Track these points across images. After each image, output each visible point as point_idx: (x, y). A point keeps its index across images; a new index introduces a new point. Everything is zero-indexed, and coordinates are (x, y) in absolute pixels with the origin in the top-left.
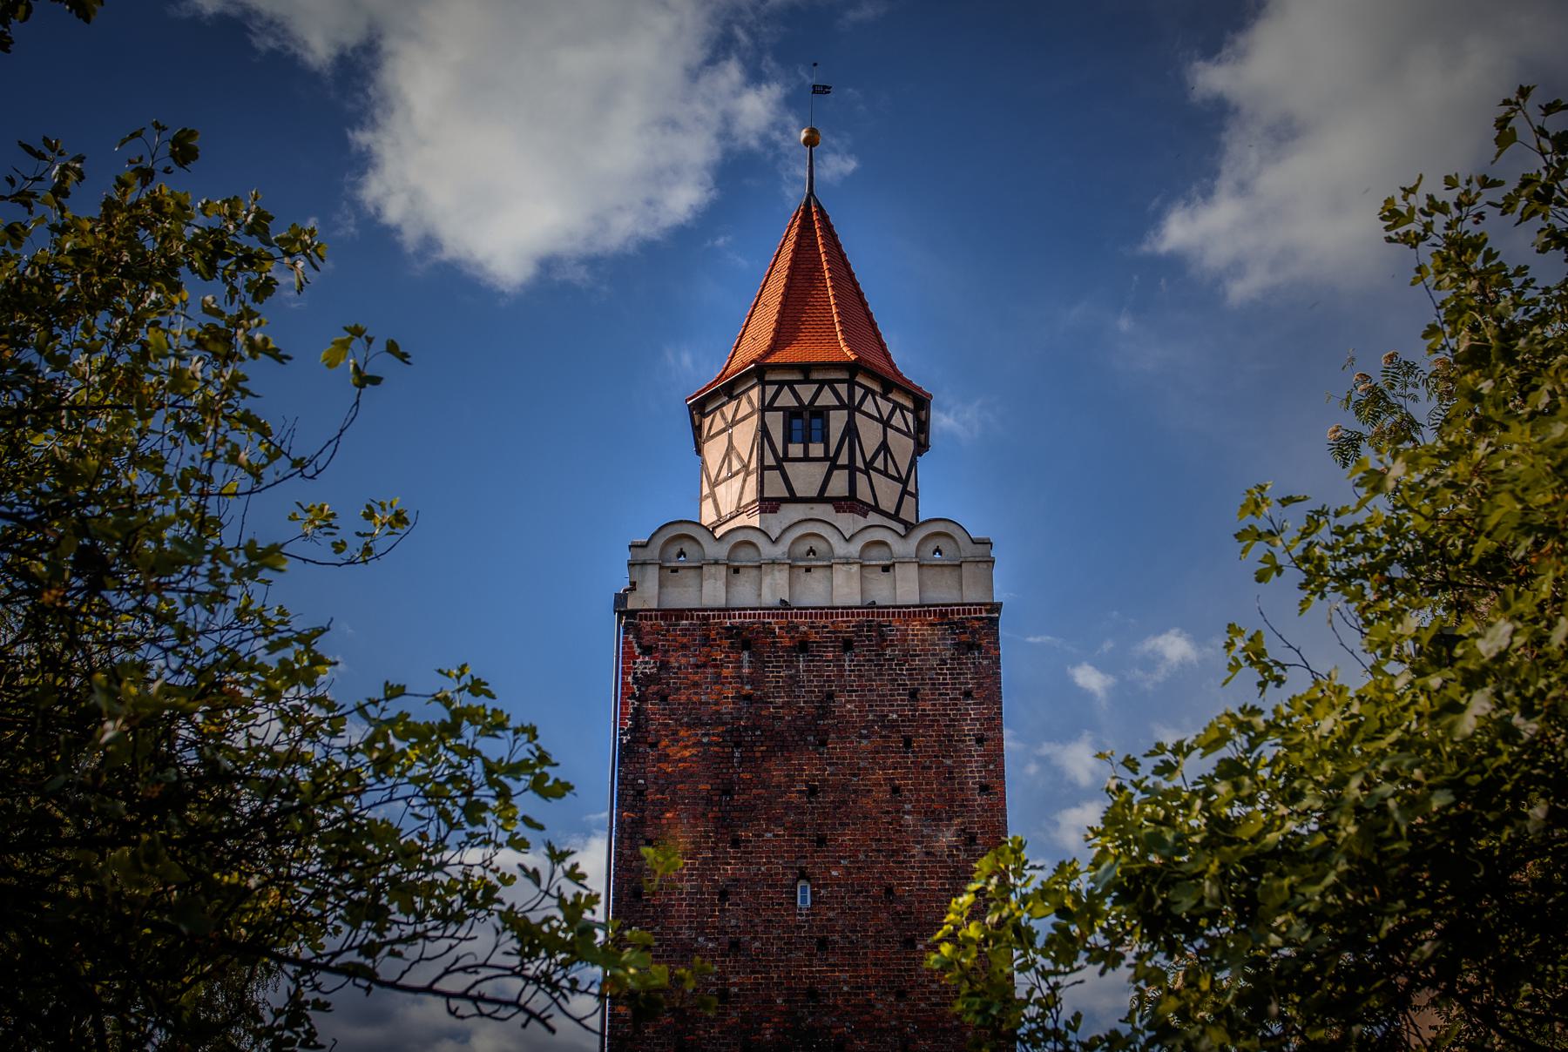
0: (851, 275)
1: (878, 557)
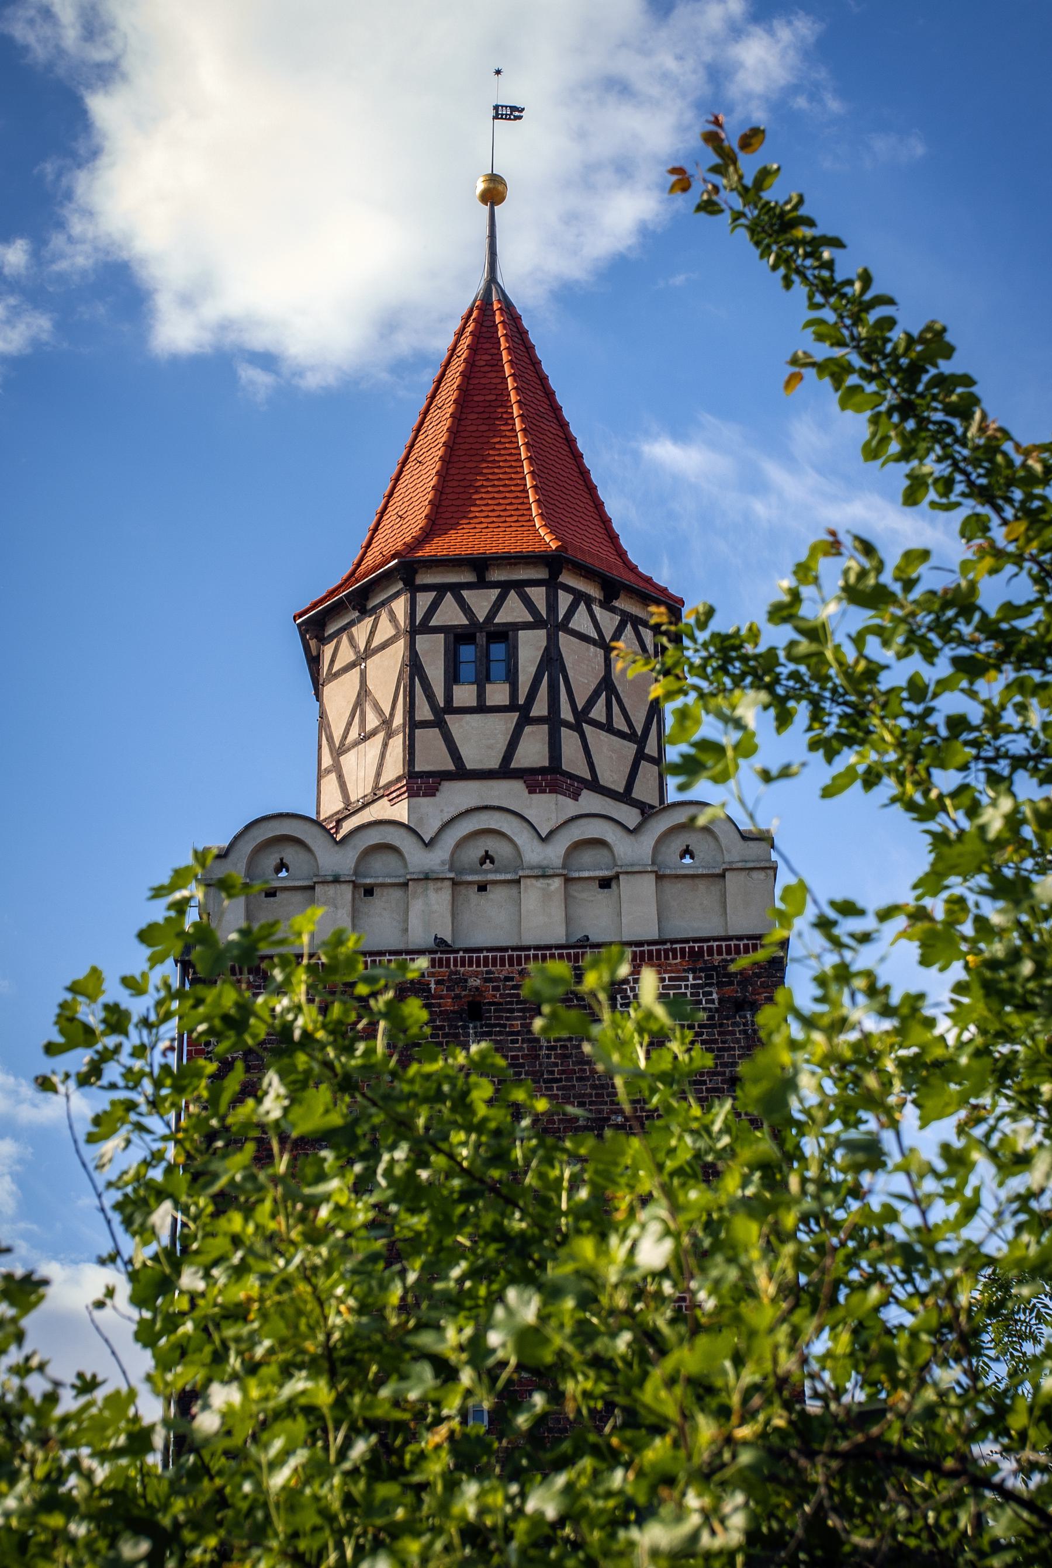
0: (556, 410)
1: (592, 864)
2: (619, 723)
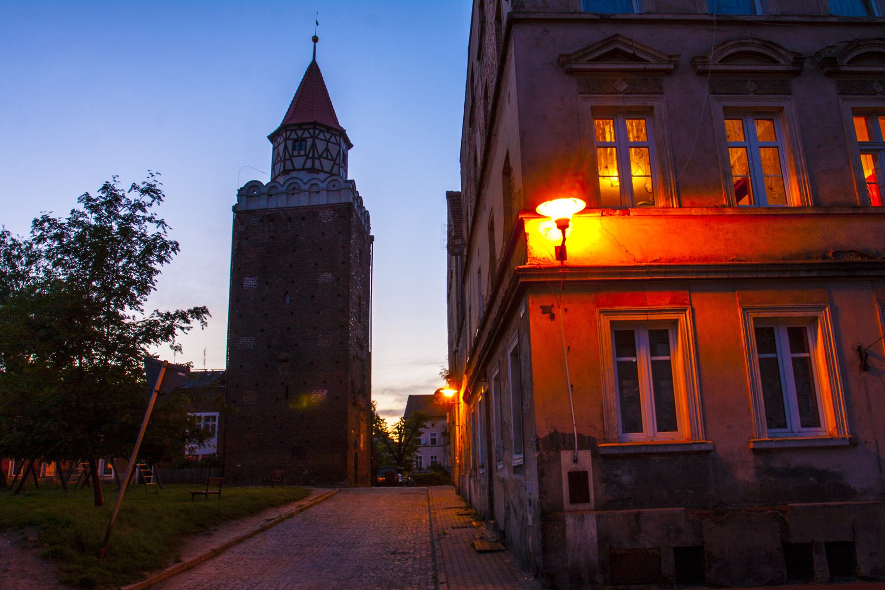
1: (315, 189)
2: (330, 157)
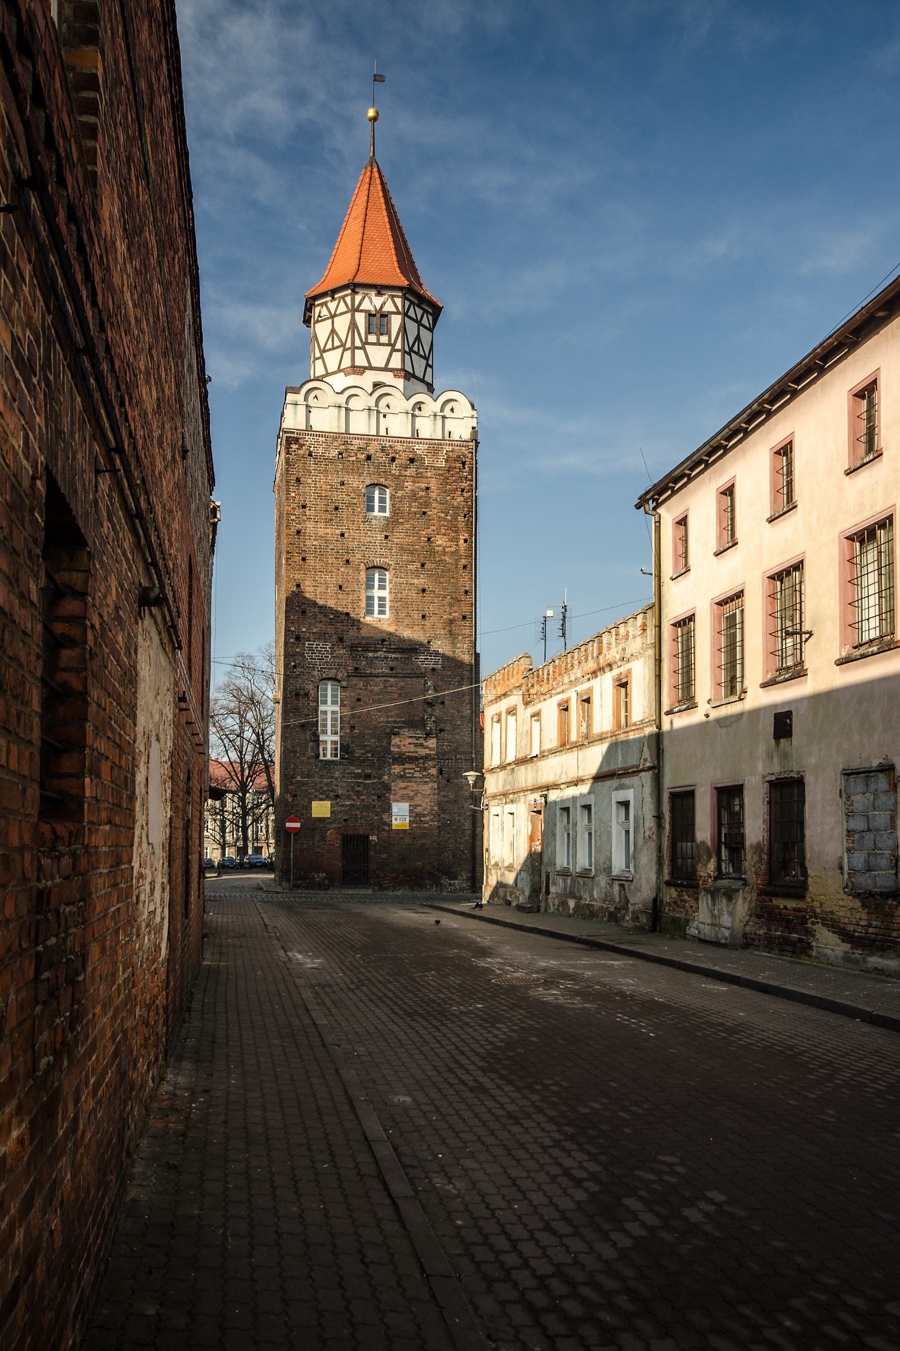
2: (422, 353)
